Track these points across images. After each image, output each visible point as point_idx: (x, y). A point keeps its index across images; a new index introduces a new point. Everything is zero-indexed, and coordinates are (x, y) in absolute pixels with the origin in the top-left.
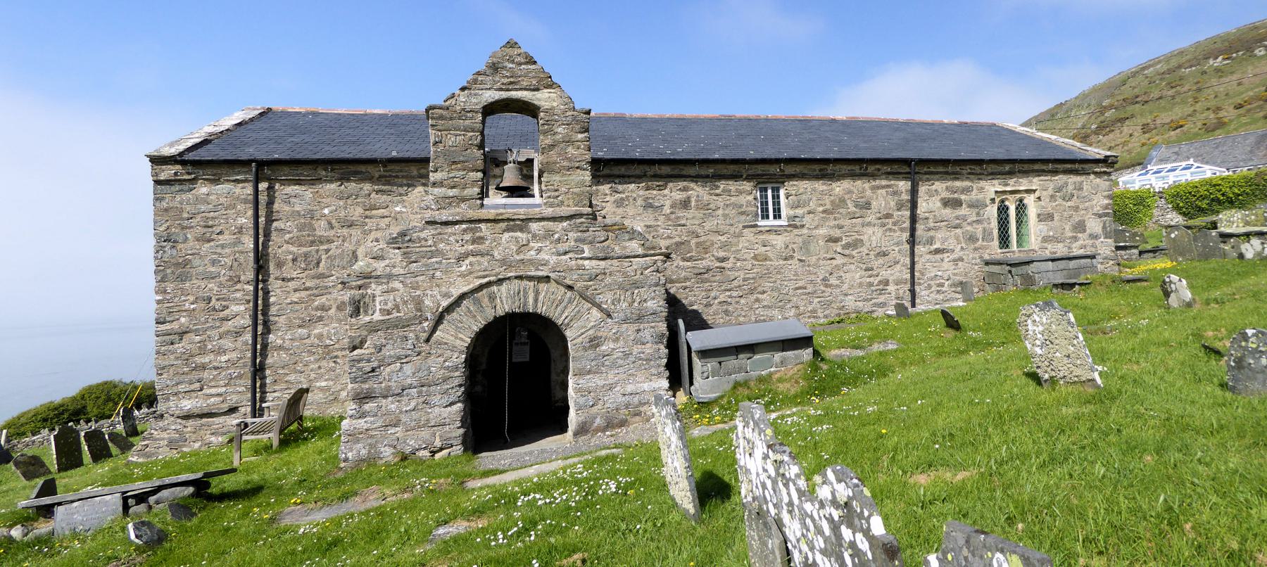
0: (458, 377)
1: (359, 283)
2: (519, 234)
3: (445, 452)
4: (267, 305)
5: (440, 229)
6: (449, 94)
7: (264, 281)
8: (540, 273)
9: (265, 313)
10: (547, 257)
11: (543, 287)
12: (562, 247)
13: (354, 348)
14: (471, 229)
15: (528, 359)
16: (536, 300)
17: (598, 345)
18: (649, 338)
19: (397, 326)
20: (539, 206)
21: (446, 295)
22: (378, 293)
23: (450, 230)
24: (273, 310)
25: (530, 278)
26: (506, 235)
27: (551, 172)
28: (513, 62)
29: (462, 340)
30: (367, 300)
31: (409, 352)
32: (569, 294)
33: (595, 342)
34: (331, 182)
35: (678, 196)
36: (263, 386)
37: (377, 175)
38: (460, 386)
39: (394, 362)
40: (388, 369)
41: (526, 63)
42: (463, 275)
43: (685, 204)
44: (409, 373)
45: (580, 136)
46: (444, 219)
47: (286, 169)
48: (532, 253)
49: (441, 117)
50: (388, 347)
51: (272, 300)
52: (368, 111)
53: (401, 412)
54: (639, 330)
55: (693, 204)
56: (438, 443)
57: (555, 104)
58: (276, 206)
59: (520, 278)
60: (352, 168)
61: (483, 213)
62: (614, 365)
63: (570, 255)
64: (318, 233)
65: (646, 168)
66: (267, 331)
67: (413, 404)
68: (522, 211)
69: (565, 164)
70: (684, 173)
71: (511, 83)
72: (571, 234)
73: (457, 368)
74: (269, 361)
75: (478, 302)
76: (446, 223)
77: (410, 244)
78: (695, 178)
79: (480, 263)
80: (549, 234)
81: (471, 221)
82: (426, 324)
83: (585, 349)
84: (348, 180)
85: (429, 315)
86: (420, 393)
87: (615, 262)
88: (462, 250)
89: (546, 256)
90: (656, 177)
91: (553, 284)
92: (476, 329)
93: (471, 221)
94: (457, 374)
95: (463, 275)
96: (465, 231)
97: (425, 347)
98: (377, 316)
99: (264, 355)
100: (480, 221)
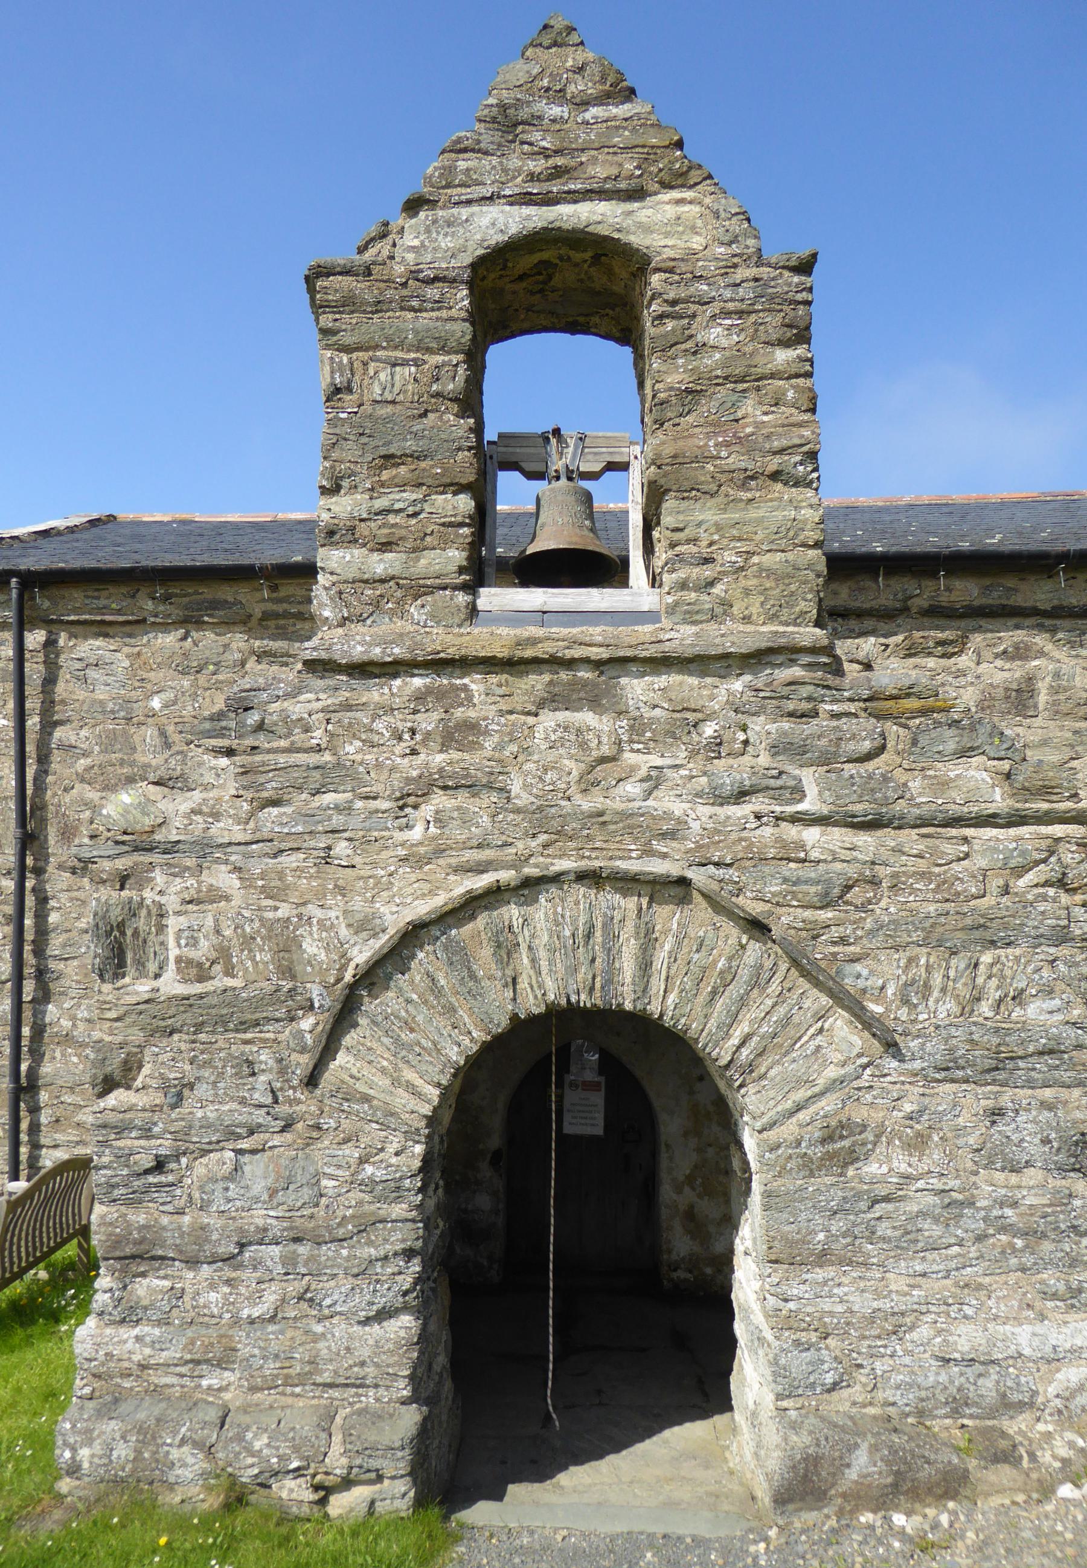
0: (401, 1222)
1: (122, 864)
2: (587, 717)
3: (359, 1494)
4: (42, 931)
5: (346, 689)
6: (373, 230)
7: (39, 871)
8: (658, 867)
9: (39, 952)
10: (678, 808)
11: (668, 918)
12: (731, 772)
13: (108, 1085)
14: (440, 695)
15: (599, 1131)
16: (645, 966)
17: (851, 1158)
18: (1033, 1148)
19: (222, 1021)
20: (650, 616)
21: (365, 926)
22: (171, 902)
23: (375, 693)
24: (55, 945)
25: (627, 883)
26: (549, 720)
27: (691, 491)
28: (559, 95)
29: (416, 1093)
30: (141, 923)
31: (260, 1117)
32: (754, 949)
33: (840, 1145)
34: (164, 627)
35: (1000, 674)
36: (35, 1128)
37: (257, 611)
38: (409, 1254)
39: (216, 1146)
40: (201, 1168)
41: (604, 99)
42: (413, 859)
43: (1020, 699)
44: (259, 1188)
45: (783, 356)
46: (358, 652)
47: (77, 596)
48: (632, 788)
49: (348, 304)
50: (203, 1090)
51: (53, 918)
52: (281, 516)
53: (236, 1321)
54: (996, 1114)
55: (1043, 698)
56: (337, 1462)
57: (697, 242)
58: (61, 689)
59: (591, 878)
60: (207, 592)
61: (480, 640)
62: (908, 1241)
63: (758, 803)
64: (141, 758)
65: (907, 585)
66: (44, 996)
67: (270, 1298)
68: (596, 633)
69: (735, 460)
70: (1017, 600)
71: (558, 173)
72: (759, 726)
73: (396, 1192)
74: (47, 1069)
75: (460, 959)
76: (364, 670)
77: (261, 740)
78: (1049, 617)
79: (466, 821)
80: (686, 719)
81: (438, 665)
82: (307, 1023)
83: (810, 1167)
84: (199, 624)
85: (315, 992)
86: (289, 1261)
87: (909, 838)
88: (412, 768)
89: (676, 802)
90: (937, 613)
91: (700, 909)
92: (455, 1055)
93: (438, 665)
94: (399, 1210)
95: (413, 859)
96: (420, 697)
97: (306, 1105)
98: (171, 984)
99: (37, 1056)
100: (464, 664)
